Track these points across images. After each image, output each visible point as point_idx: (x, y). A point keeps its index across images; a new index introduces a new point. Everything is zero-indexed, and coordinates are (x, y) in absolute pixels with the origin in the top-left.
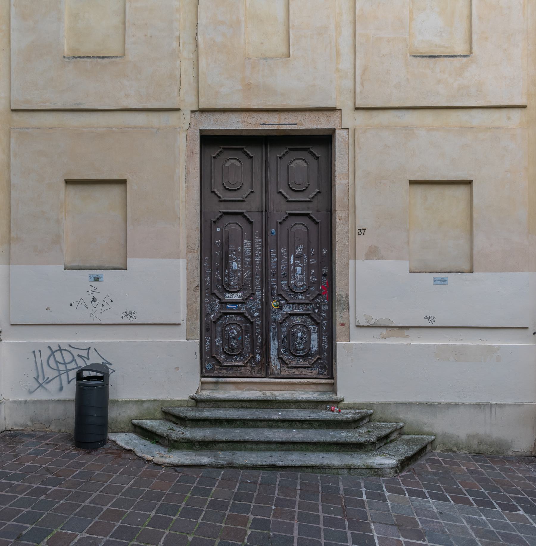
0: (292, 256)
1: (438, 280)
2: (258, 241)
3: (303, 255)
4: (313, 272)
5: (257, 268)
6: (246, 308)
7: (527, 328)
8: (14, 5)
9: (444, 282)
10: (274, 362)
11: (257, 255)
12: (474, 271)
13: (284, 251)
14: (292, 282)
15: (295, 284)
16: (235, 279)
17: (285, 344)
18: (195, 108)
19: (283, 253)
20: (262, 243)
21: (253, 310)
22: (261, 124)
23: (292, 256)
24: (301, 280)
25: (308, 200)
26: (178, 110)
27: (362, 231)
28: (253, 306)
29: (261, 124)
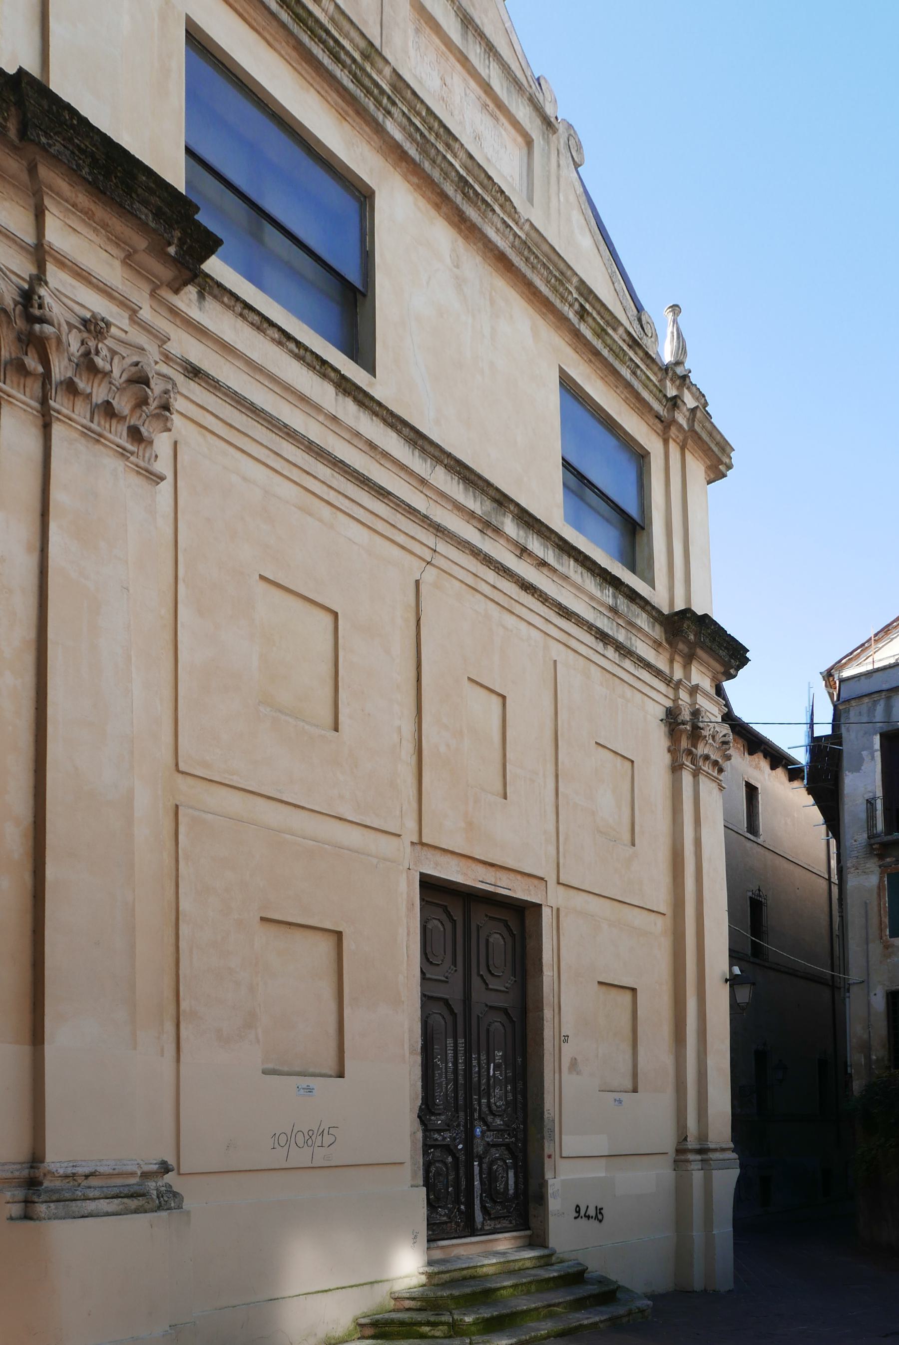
0: (492, 1065)
1: (304, 1089)
2: (461, 1041)
3: (501, 1063)
4: (509, 1087)
5: (461, 1080)
6: (450, 1137)
7: (667, 1153)
8: (184, 581)
9: (310, 1092)
10: (479, 1216)
11: (460, 1061)
12: (639, 1090)
13: (483, 1057)
14: (492, 1100)
15: (495, 1104)
16: (440, 1096)
17: (486, 1187)
18: (415, 840)
19: (483, 1060)
20: (465, 1045)
21: (458, 1140)
22: (480, 881)
23: (492, 1065)
24: (500, 1099)
25: (504, 989)
26: (399, 836)
27: (566, 1038)
28: (457, 1134)
29: (480, 881)
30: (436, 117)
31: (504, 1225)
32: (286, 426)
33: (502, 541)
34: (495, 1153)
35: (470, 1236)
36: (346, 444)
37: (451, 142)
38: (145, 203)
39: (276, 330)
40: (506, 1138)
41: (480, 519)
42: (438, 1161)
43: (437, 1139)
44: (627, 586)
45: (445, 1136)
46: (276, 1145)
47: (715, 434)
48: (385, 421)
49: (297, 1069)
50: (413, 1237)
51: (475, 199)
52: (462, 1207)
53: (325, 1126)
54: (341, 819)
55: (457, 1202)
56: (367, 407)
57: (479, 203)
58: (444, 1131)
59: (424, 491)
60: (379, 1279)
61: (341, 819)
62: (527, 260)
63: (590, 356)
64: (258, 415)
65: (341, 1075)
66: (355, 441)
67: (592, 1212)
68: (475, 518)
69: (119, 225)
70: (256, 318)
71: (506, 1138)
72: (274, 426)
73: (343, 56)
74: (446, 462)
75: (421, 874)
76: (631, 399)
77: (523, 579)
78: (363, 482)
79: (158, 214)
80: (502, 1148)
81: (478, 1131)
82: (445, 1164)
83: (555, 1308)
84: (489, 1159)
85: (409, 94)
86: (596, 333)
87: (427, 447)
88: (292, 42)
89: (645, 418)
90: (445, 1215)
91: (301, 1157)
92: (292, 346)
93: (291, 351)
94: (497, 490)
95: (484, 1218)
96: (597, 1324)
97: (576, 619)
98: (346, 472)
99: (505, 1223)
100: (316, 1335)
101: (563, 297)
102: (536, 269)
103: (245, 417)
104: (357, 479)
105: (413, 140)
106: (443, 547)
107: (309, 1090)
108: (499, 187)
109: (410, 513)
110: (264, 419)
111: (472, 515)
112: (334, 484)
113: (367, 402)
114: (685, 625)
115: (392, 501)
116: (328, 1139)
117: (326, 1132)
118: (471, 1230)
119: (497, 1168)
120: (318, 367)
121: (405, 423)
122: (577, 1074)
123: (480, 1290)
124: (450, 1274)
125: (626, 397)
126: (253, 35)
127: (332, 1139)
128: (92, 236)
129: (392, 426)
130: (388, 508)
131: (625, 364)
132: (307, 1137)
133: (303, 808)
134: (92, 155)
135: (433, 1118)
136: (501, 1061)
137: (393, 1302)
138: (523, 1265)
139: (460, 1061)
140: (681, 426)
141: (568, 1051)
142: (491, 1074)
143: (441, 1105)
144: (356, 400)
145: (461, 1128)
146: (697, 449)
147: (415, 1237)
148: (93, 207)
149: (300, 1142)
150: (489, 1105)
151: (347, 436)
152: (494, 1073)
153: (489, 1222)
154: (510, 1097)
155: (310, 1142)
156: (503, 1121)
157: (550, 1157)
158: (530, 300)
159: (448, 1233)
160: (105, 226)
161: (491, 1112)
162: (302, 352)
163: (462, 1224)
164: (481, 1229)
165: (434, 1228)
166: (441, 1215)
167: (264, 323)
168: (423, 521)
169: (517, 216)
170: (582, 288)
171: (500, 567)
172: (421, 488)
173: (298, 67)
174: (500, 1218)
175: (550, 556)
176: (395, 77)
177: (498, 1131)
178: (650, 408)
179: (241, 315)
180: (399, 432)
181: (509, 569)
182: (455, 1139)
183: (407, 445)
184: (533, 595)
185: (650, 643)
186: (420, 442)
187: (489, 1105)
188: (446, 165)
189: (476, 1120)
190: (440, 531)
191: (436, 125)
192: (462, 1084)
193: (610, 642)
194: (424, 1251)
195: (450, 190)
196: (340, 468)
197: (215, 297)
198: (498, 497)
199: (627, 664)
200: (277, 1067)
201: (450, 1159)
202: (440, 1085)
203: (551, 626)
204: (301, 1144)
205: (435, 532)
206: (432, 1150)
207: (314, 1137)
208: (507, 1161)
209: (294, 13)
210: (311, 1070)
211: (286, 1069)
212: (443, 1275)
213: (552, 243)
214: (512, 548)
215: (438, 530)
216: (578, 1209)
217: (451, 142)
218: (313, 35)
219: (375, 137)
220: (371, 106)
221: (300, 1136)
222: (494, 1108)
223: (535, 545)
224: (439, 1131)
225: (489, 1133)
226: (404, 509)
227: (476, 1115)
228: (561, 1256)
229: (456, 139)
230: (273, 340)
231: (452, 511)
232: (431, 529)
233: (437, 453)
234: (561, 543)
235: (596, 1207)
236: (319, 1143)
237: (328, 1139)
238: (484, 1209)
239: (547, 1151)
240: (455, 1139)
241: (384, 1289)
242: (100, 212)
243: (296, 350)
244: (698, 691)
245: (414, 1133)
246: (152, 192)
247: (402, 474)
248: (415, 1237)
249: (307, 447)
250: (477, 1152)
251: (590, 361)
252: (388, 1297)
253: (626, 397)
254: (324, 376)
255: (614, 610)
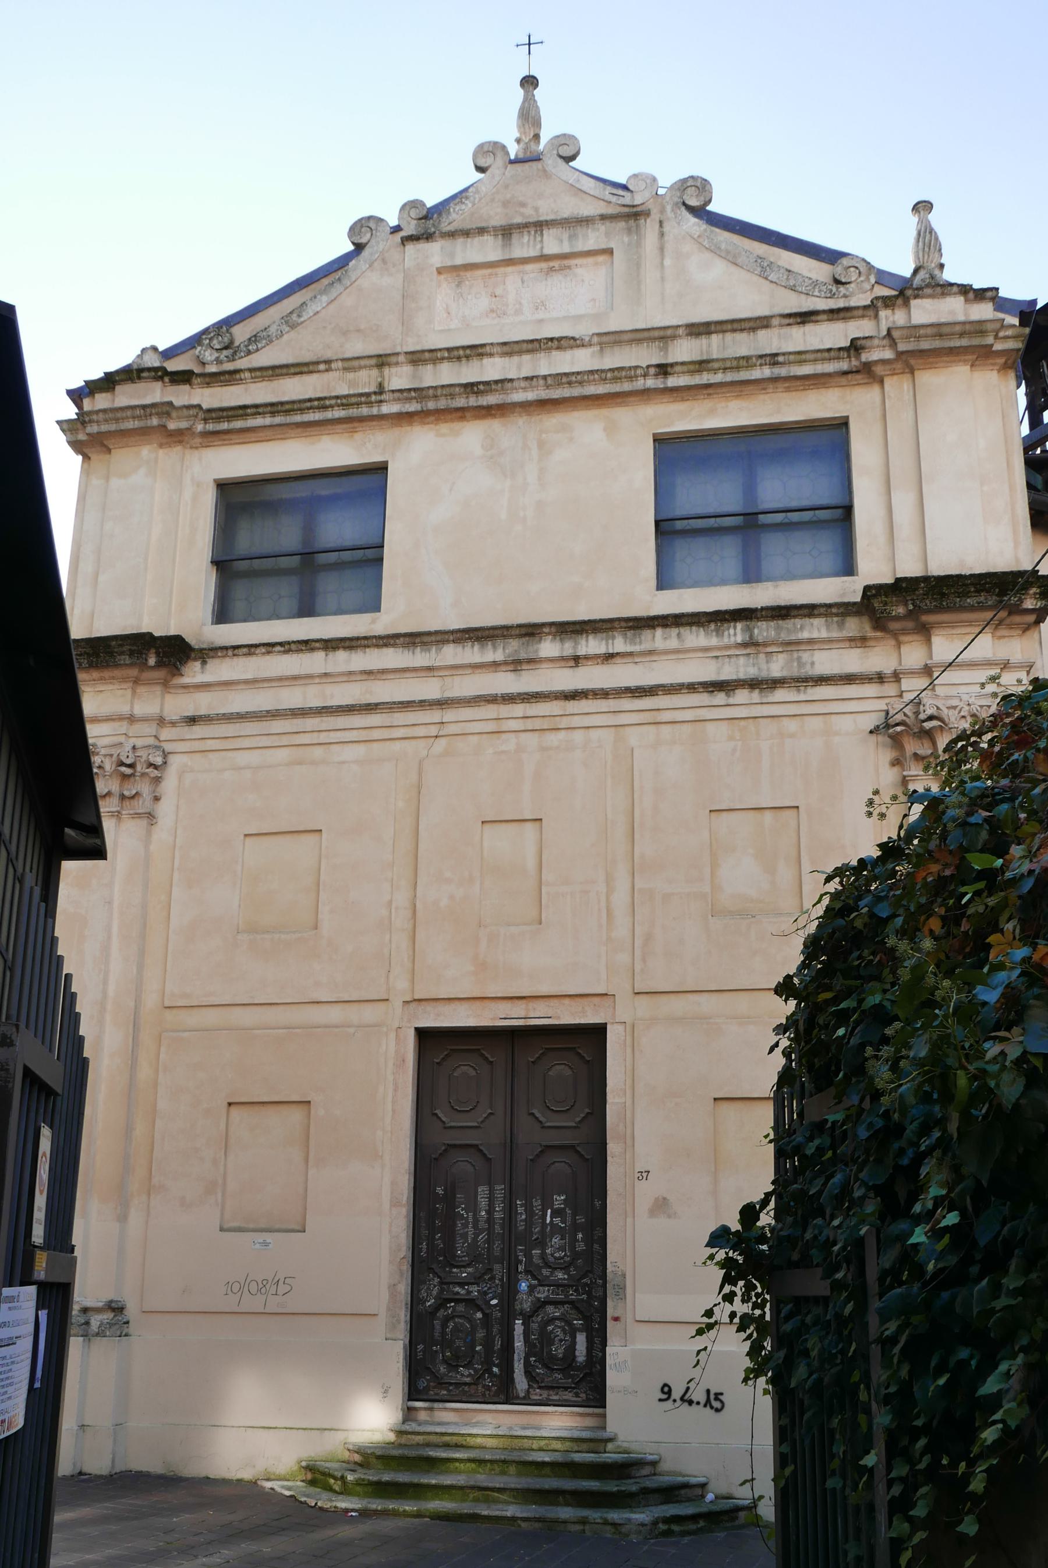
0: (549, 1211)
3: (564, 1209)
6: (478, 1291)
10: (521, 1383)
11: (497, 1209)
15: (552, 1255)
16: (463, 1247)
23: (549, 1211)
27: (645, 1175)
28: (489, 1288)
30: (457, 348)
31: (565, 1397)
32: (268, 712)
33: (544, 665)
34: (552, 1311)
35: (506, 1403)
36: (347, 684)
37: (480, 351)
38: (122, 653)
39: (261, 648)
40: (572, 1295)
41: (505, 663)
42: (459, 1317)
43: (458, 1293)
44: (762, 609)
45: (471, 1289)
46: (229, 1292)
47: (946, 330)
48: (377, 646)
49: (263, 1226)
50: (383, 1391)
51: (487, 388)
52: (495, 1369)
53: (281, 1276)
54: (318, 1002)
55: (488, 1364)
56: (357, 647)
57: (493, 387)
58: (468, 1284)
59: (436, 674)
60: (334, 1427)
61: (318, 1002)
62: (570, 383)
63: (705, 392)
64: (247, 718)
65: (222, 1230)
66: (353, 678)
67: (699, 1395)
68: (500, 664)
69: (117, 673)
70: (245, 650)
71: (572, 1295)
72: (260, 717)
73: (328, 403)
74: (451, 638)
75: (416, 1029)
76: (794, 384)
77: (563, 691)
78: (350, 711)
79: (131, 654)
80: (565, 1306)
81: (524, 1286)
82: (470, 1320)
83: (496, 1494)
84: (542, 1318)
85: (427, 355)
86: (692, 372)
87: (426, 639)
88: (293, 426)
89: (833, 384)
90: (470, 1375)
91: (255, 1303)
92: (278, 648)
93: (279, 652)
94: (520, 626)
95: (529, 1385)
96: (515, 1521)
97: (662, 690)
98: (331, 712)
99: (568, 1396)
100: (254, 1466)
101: (631, 377)
102: (584, 381)
103: (238, 724)
104: (343, 711)
105: (409, 400)
106: (450, 715)
107: (266, 1244)
108: (546, 339)
109: (404, 707)
110: (252, 717)
111: (495, 665)
112: (324, 727)
113: (354, 643)
114: (875, 605)
115: (383, 709)
116: (282, 1288)
117: (281, 1282)
118: (505, 1394)
119: (553, 1329)
120: (304, 648)
121: (397, 636)
122: (669, 1217)
123: (414, 1455)
124: (425, 1437)
125: (785, 388)
126: (270, 443)
127: (288, 1288)
128: (111, 687)
129: (386, 645)
130: (384, 715)
131: (755, 366)
132: (261, 1286)
133: (277, 1004)
134: (85, 653)
135: (455, 1270)
136: (562, 1206)
137: (347, 1453)
138: (547, 1445)
139: (497, 1209)
140: (883, 362)
141: (646, 1193)
142: (548, 1222)
143: (464, 1256)
144: (345, 648)
145: (497, 1282)
146: (934, 360)
147: (386, 1392)
148: (102, 675)
149: (254, 1290)
150: (543, 1256)
151: (345, 679)
152: (551, 1220)
153: (538, 1390)
154: (581, 1247)
155: (263, 1290)
156: (569, 1275)
157: (616, 1319)
158: (598, 405)
159: (471, 1395)
160: (113, 678)
161: (547, 1265)
162: (287, 647)
163: (494, 1389)
164: (524, 1398)
165: (451, 1388)
166: (462, 1375)
167: (251, 649)
168: (422, 706)
169: (578, 342)
170: (695, 330)
171: (526, 696)
172: (432, 674)
173: (308, 434)
174: (558, 1388)
175: (619, 644)
176: (409, 357)
177: (558, 1286)
178: (829, 375)
179: (234, 655)
180: (394, 645)
181: (537, 693)
182: (486, 1293)
183: (406, 651)
184: (587, 698)
185: (847, 644)
186: (418, 640)
187: (543, 1256)
188: (448, 389)
189: (521, 1273)
190: (444, 704)
191: (461, 352)
192: (498, 1233)
193: (734, 686)
194: (397, 1408)
195: (460, 402)
196: (326, 712)
197: (213, 657)
198: (523, 631)
199: (781, 694)
200: (243, 1225)
201: (479, 1315)
202: (465, 1236)
203: (622, 715)
204: (254, 1291)
205: (439, 707)
206: (453, 1304)
207: (268, 1286)
208: (575, 1322)
209: (283, 412)
210: (277, 1226)
211: (251, 1226)
212: (413, 1437)
213: (630, 328)
214: (563, 664)
215: (440, 705)
216: (666, 1391)
217: (480, 351)
218: (302, 410)
219: (383, 422)
220: (365, 411)
221: (253, 1285)
222: (551, 1259)
223: (592, 645)
224: (461, 1285)
225: (541, 1288)
226: (399, 708)
227: (521, 1268)
228: (625, 1445)
229: (483, 346)
230: (263, 654)
231: (473, 673)
232: (434, 707)
233: (439, 638)
234: (631, 624)
235: (708, 1391)
236: (273, 1290)
237: (282, 1288)
238: (529, 1373)
239: (610, 1312)
240: (486, 1293)
241: (340, 1436)
242: (107, 674)
243: (283, 649)
244: (901, 676)
245: (394, 1285)
246: (121, 645)
247: (407, 675)
248: (386, 1392)
249: (292, 715)
250: (522, 1310)
251: (709, 394)
252: (342, 1447)
253: (785, 388)
254: (313, 649)
255: (751, 644)
